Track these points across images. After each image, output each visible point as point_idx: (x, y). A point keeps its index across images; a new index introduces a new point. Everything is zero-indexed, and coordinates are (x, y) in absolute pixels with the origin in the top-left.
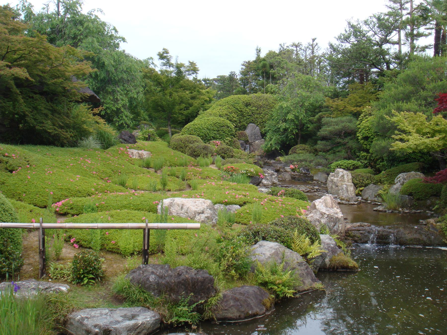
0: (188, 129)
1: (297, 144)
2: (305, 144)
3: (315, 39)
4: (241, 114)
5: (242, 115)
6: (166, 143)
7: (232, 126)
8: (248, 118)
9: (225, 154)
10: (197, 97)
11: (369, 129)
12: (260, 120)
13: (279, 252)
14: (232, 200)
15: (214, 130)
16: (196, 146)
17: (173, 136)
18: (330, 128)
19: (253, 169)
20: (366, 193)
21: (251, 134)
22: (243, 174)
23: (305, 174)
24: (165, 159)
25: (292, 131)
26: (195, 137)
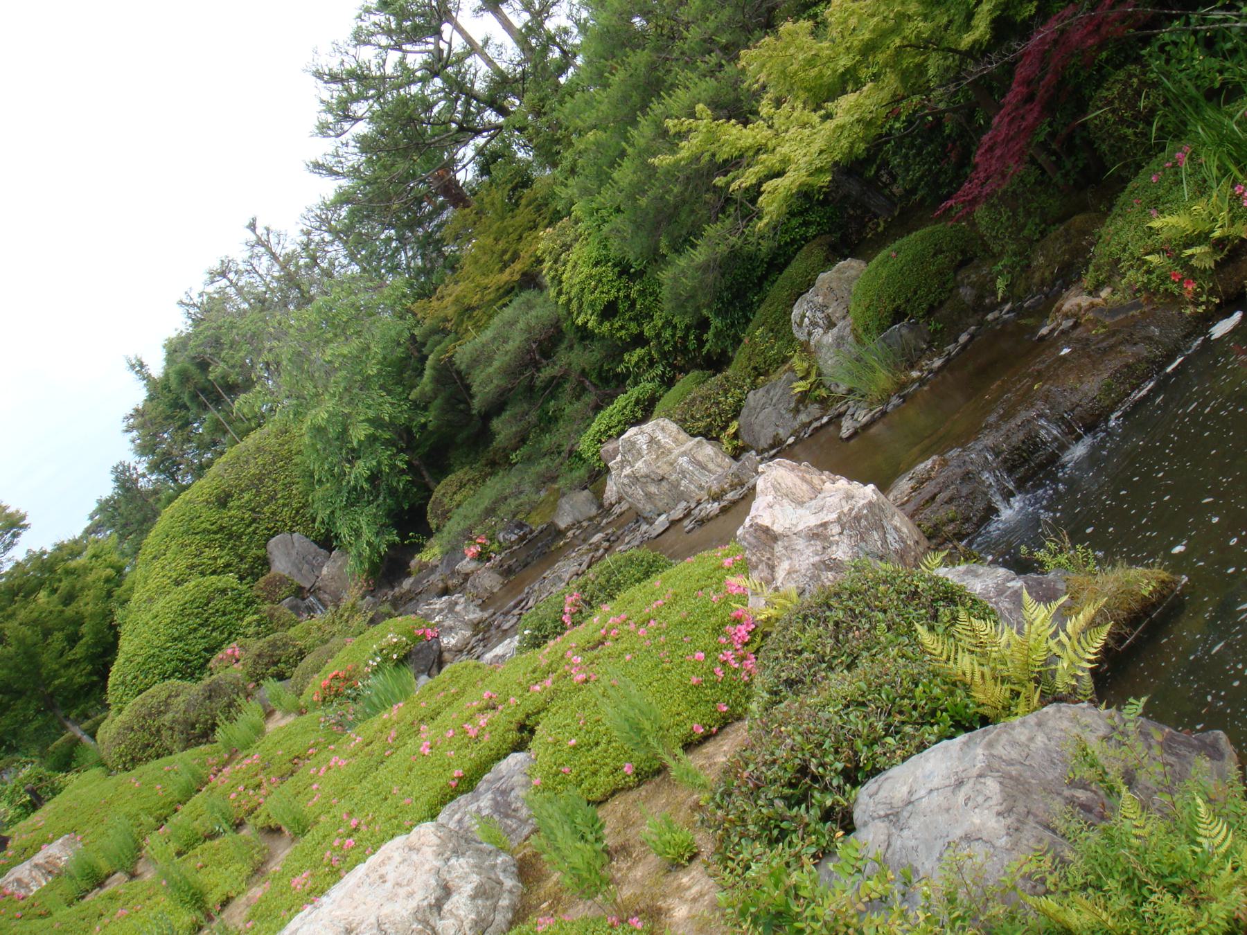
0: (123, 683)
1: (430, 492)
2: (454, 472)
3: (254, 220)
4: (230, 535)
5: (231, 536)
6: (96, 771)
7: (230, 579)
8: (254, 532)
9: (275, 664)
10: (78, 587)
11: (600, 281)
12: (286, 513)
13: (1014, 771)
14: (473, 755)
15: (195, 630)
16: (182, 707)
17: (99, 737)
18: (496, 364)
19: (392, 633)
20: (757, 428)
21: (294, 565)
22: (377, 670)
23: (521, 539)
24: (128, 816)
25: (393, 467)
26: (160, 690)
